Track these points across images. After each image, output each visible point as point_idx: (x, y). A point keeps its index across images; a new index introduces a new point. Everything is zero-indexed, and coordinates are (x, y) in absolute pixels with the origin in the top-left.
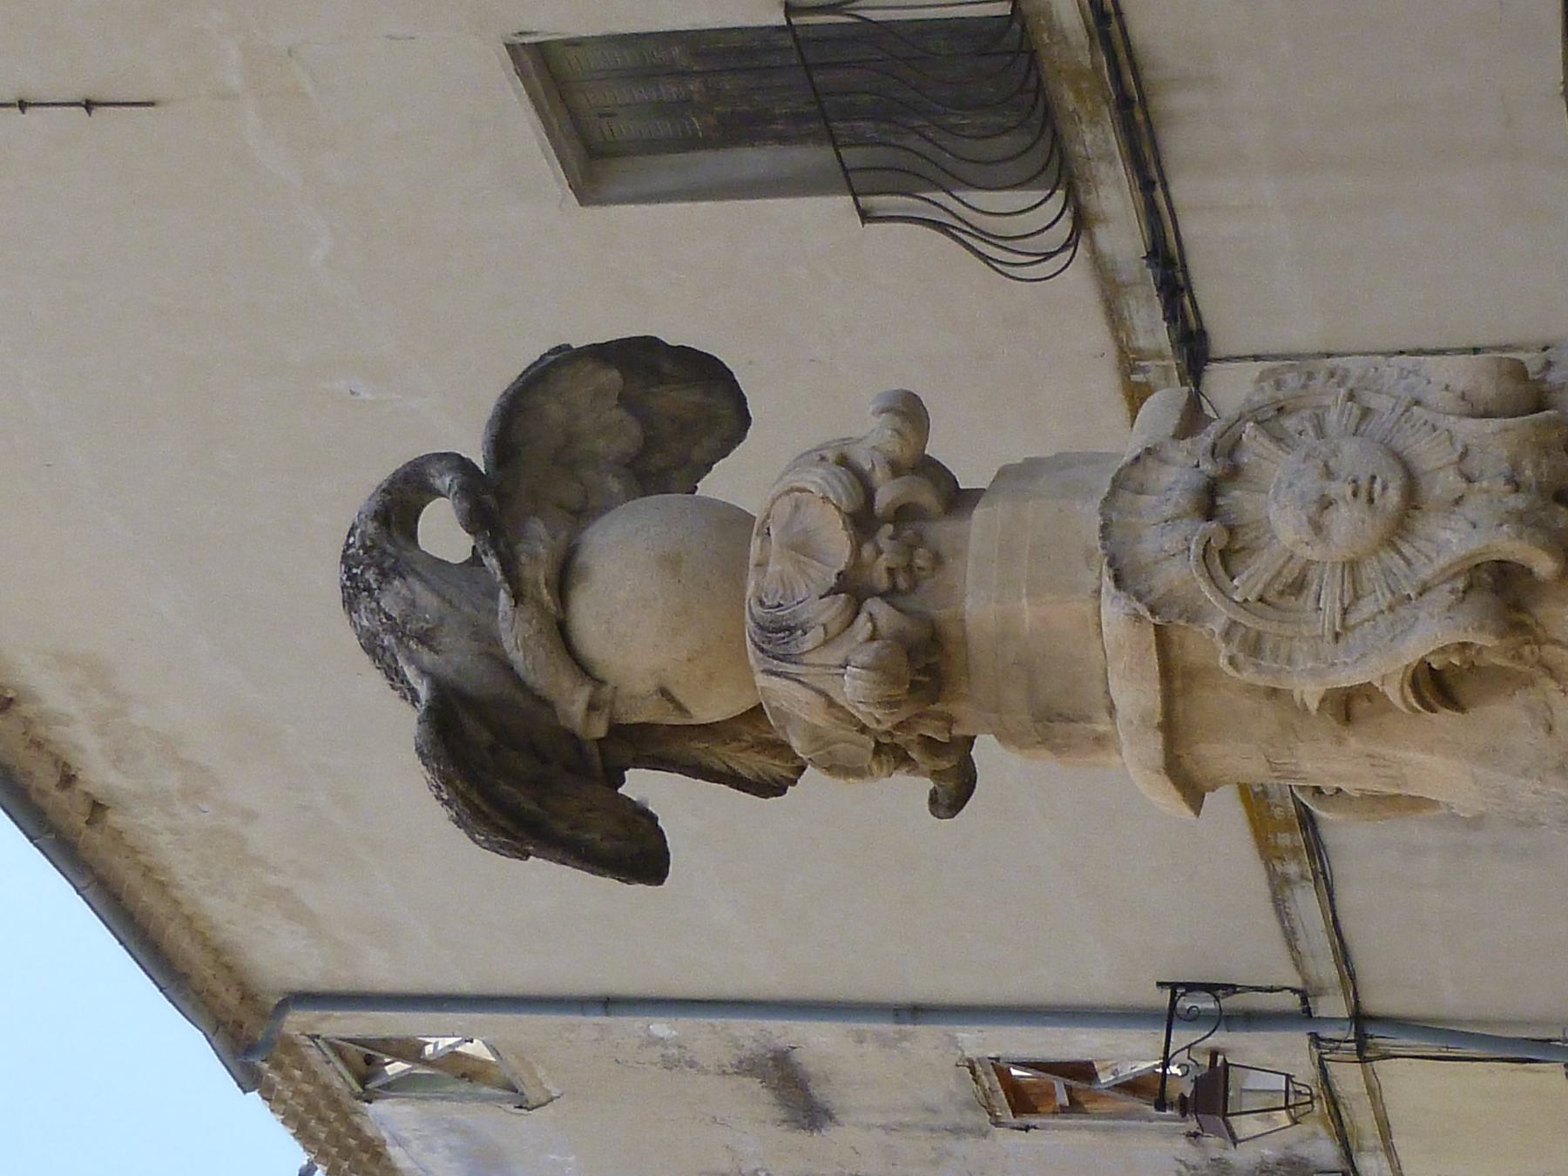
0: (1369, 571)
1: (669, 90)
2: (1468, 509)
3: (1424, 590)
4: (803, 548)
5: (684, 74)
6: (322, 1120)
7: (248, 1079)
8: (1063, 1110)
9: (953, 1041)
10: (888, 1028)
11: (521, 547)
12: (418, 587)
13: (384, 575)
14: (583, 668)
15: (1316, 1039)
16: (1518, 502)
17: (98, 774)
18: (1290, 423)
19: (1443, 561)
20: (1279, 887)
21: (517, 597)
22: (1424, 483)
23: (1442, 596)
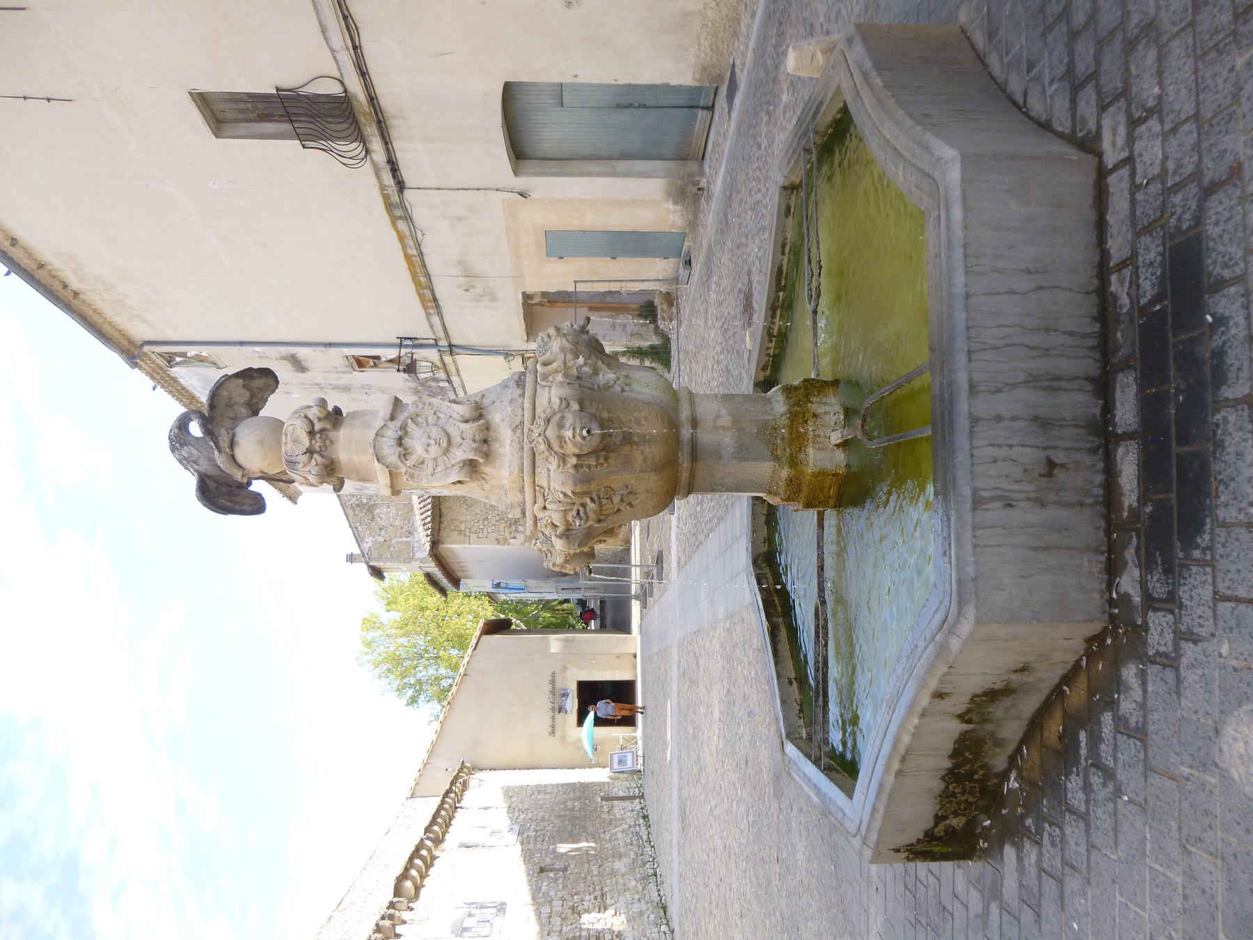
0: (440, 460)
1: (242, 106)
2: (463, 447)
3: (453, 466)
4: (296, 441)
5: (246, 102)
6: (158, 373)
7: (134, 365)
8: (372, 367)
9: (341, 352)
10: (323, 349)
11: (219, 438)
12: (192, 448)
13: (181, 445)
14: (240, 466)
15: (439, 351)
16: (475, 445)
17: (75, 284)
18: (419, 419)
19: (457, 460)
20: (428, 316)
21: (220, 452)
22: (452, 439)
23: (457, 468)
